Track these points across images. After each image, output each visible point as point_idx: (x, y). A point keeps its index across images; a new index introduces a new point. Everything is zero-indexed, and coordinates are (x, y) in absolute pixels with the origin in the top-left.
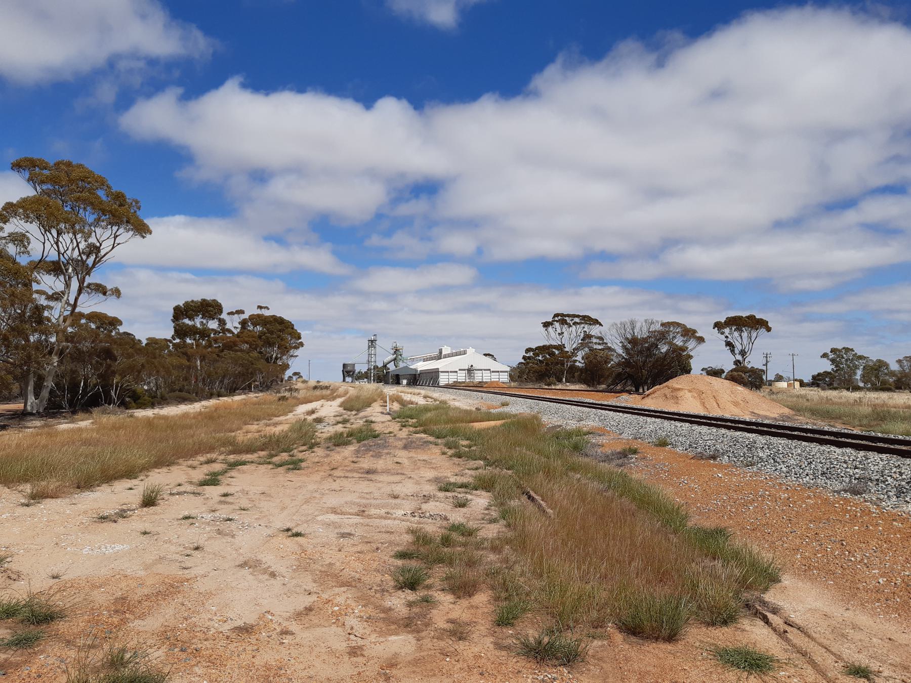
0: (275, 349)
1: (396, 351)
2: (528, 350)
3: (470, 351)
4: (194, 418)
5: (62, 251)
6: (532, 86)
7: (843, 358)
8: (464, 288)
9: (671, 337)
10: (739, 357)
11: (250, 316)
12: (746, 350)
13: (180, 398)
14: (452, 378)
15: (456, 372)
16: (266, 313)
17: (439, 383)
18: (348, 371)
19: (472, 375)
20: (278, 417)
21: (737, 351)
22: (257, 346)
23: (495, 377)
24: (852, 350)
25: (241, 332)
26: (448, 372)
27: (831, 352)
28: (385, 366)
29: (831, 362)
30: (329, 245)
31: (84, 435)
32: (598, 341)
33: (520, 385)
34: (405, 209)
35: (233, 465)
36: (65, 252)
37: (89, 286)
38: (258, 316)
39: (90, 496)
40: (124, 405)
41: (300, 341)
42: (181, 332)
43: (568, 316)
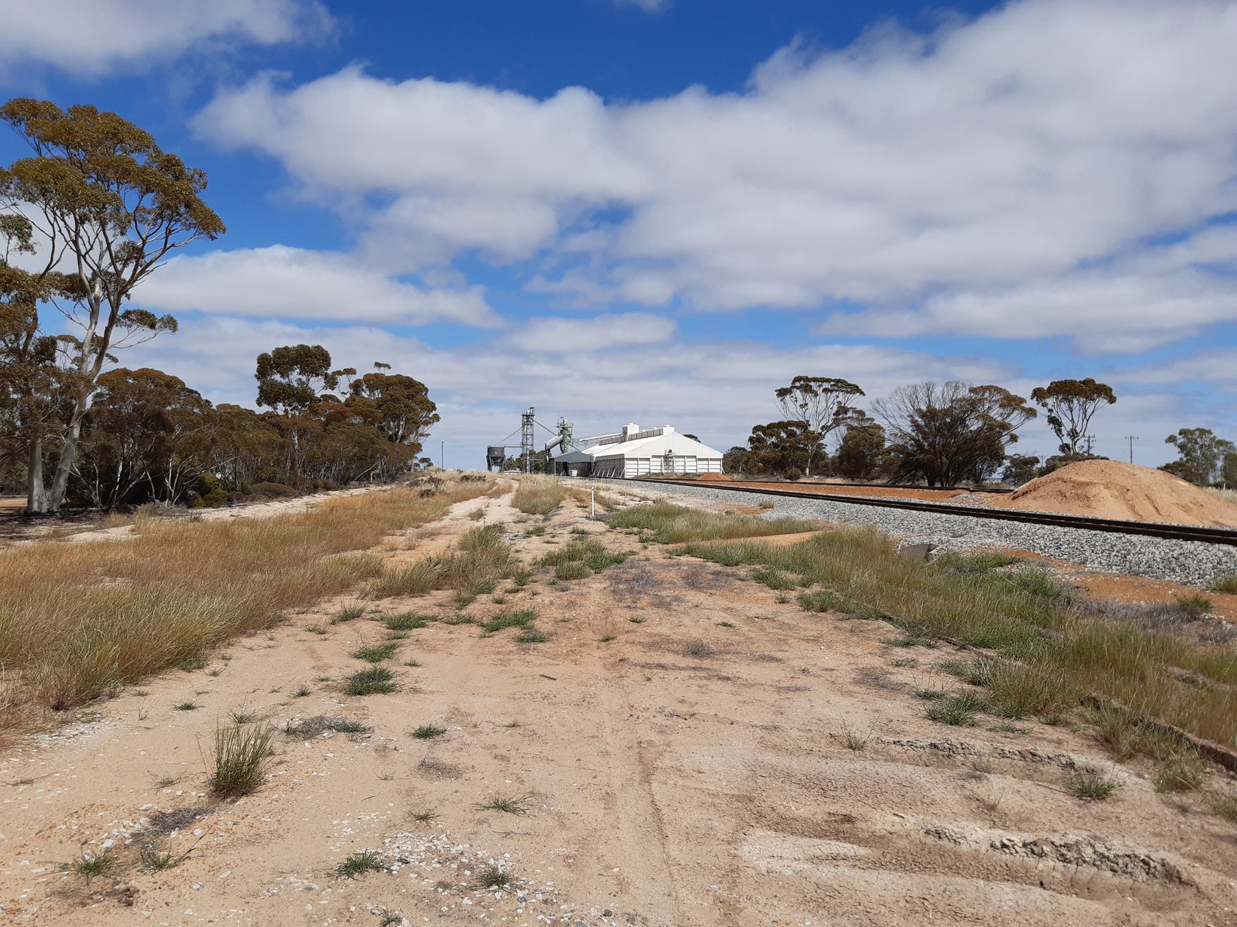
0: (401, 423)
1: (564, 430)
2: (756, 429)
3: (668, 430)
4: (299, 523)
5: (83, 251)
6: (749, 83)
7: (1196, 443)
8: (659, 347)
9: (986, 407)
10: (1067, 440)
11: (366, 375)
12: (1078, 430)
13: (270, 491)
14: (643, 469)
15: (648, 459)
16: (387, 373)
17: (624, 475)
18: (495, 458)
19: (671, 463)
20: (429, 522)
21: (1064, 432)
22: (375, 419)
23: (702, 468)
24: (1209, 432)
25: (352, 398)
26: (636, 459)
27: (1180, 434)
28: (548, 450)
29: (1179, 449)
30: (480, 289)
31: (111, 556)
32: (855, 415)
33: (747, 477)
34: (577, 243)
35: (403, 625)
36: (87, 253)
37: (127, 314)
38: (376, 375)
39: (83, 738)
40: (186, 501)
41: (434, 412)
42: (268, 395)
43: (815, 380)
